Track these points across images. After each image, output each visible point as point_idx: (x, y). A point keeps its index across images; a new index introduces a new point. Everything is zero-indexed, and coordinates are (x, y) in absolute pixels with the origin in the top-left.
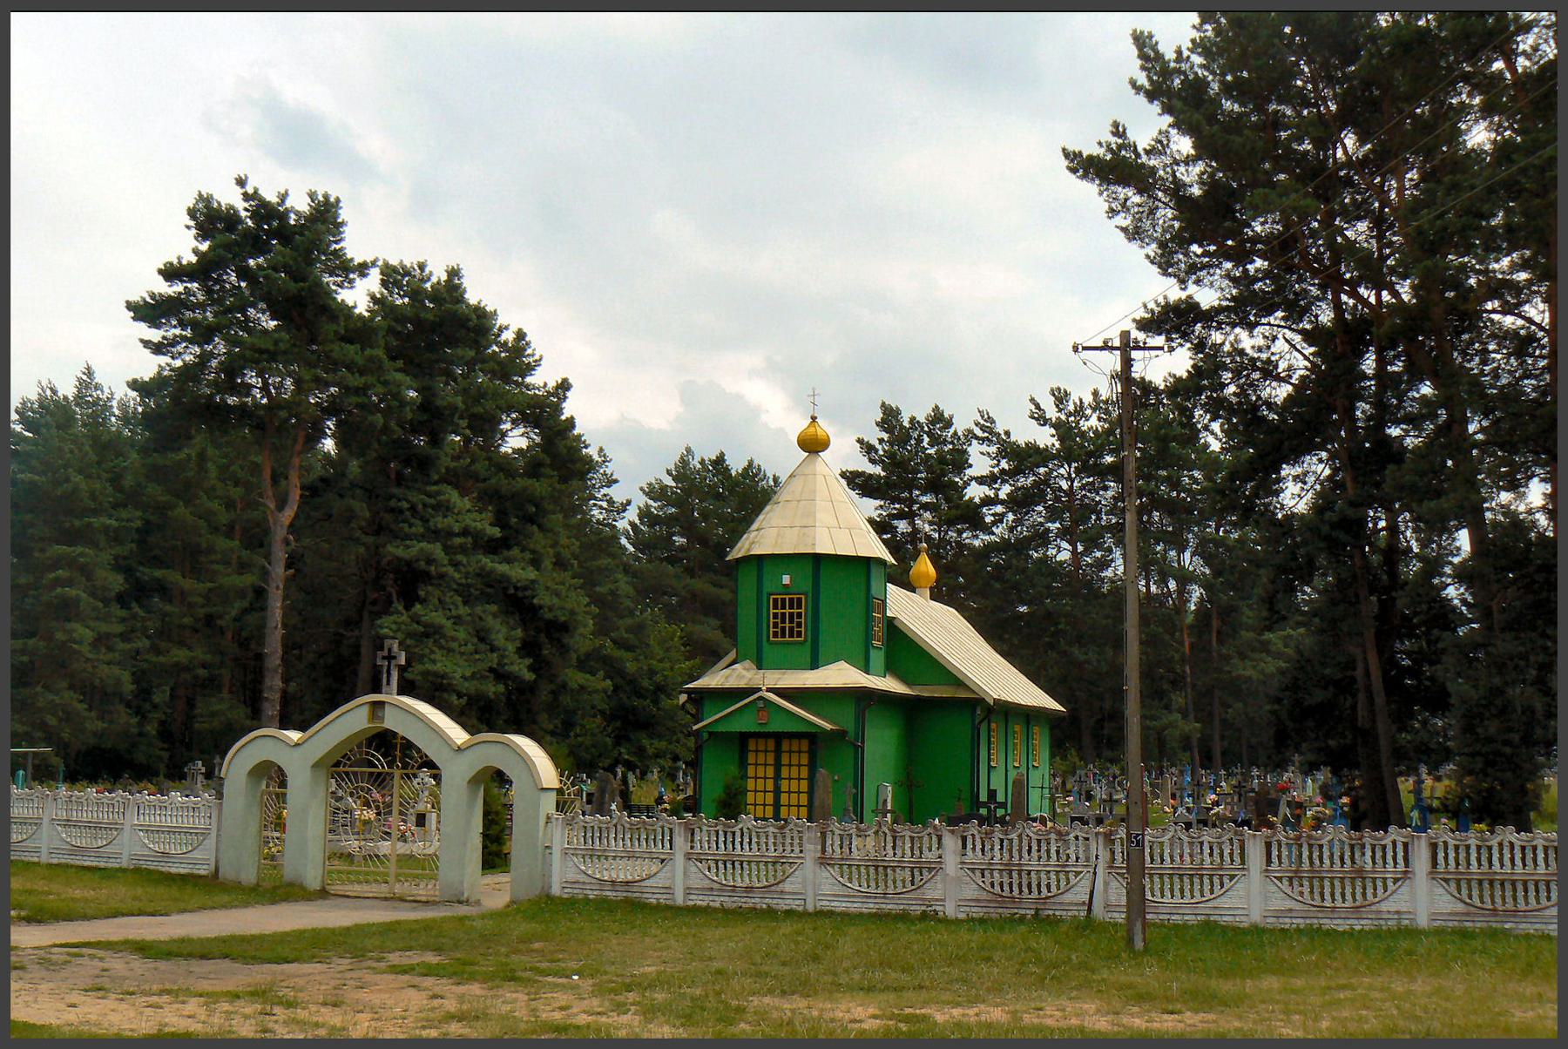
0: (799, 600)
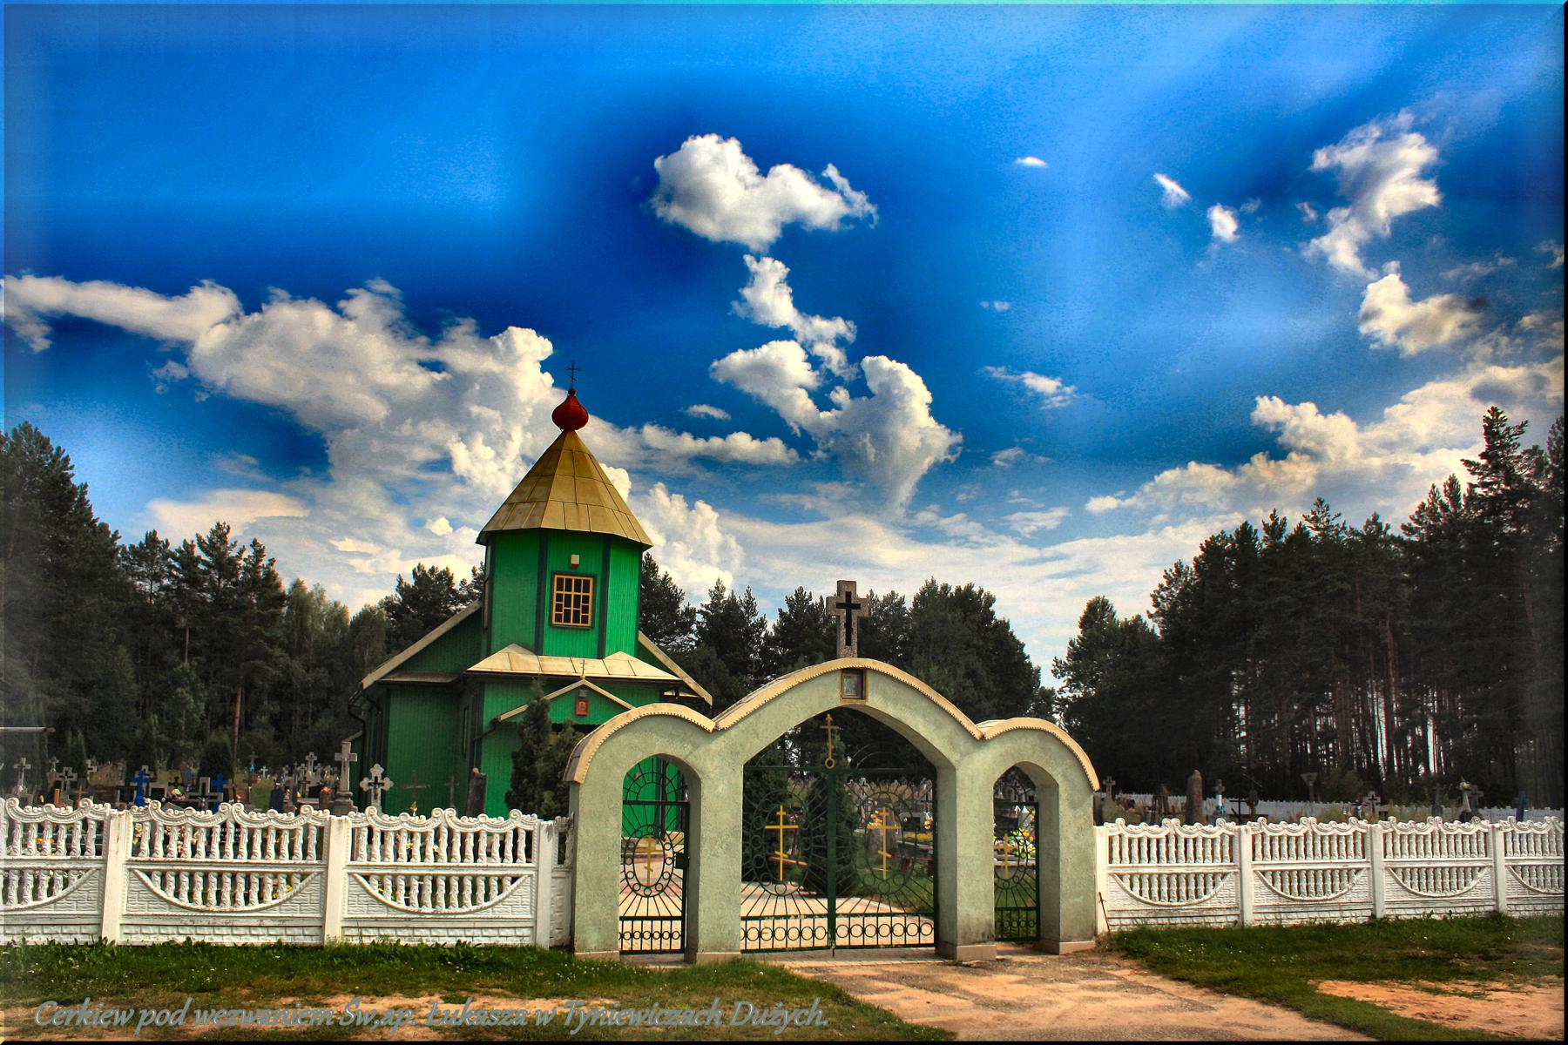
0: (587, 583)
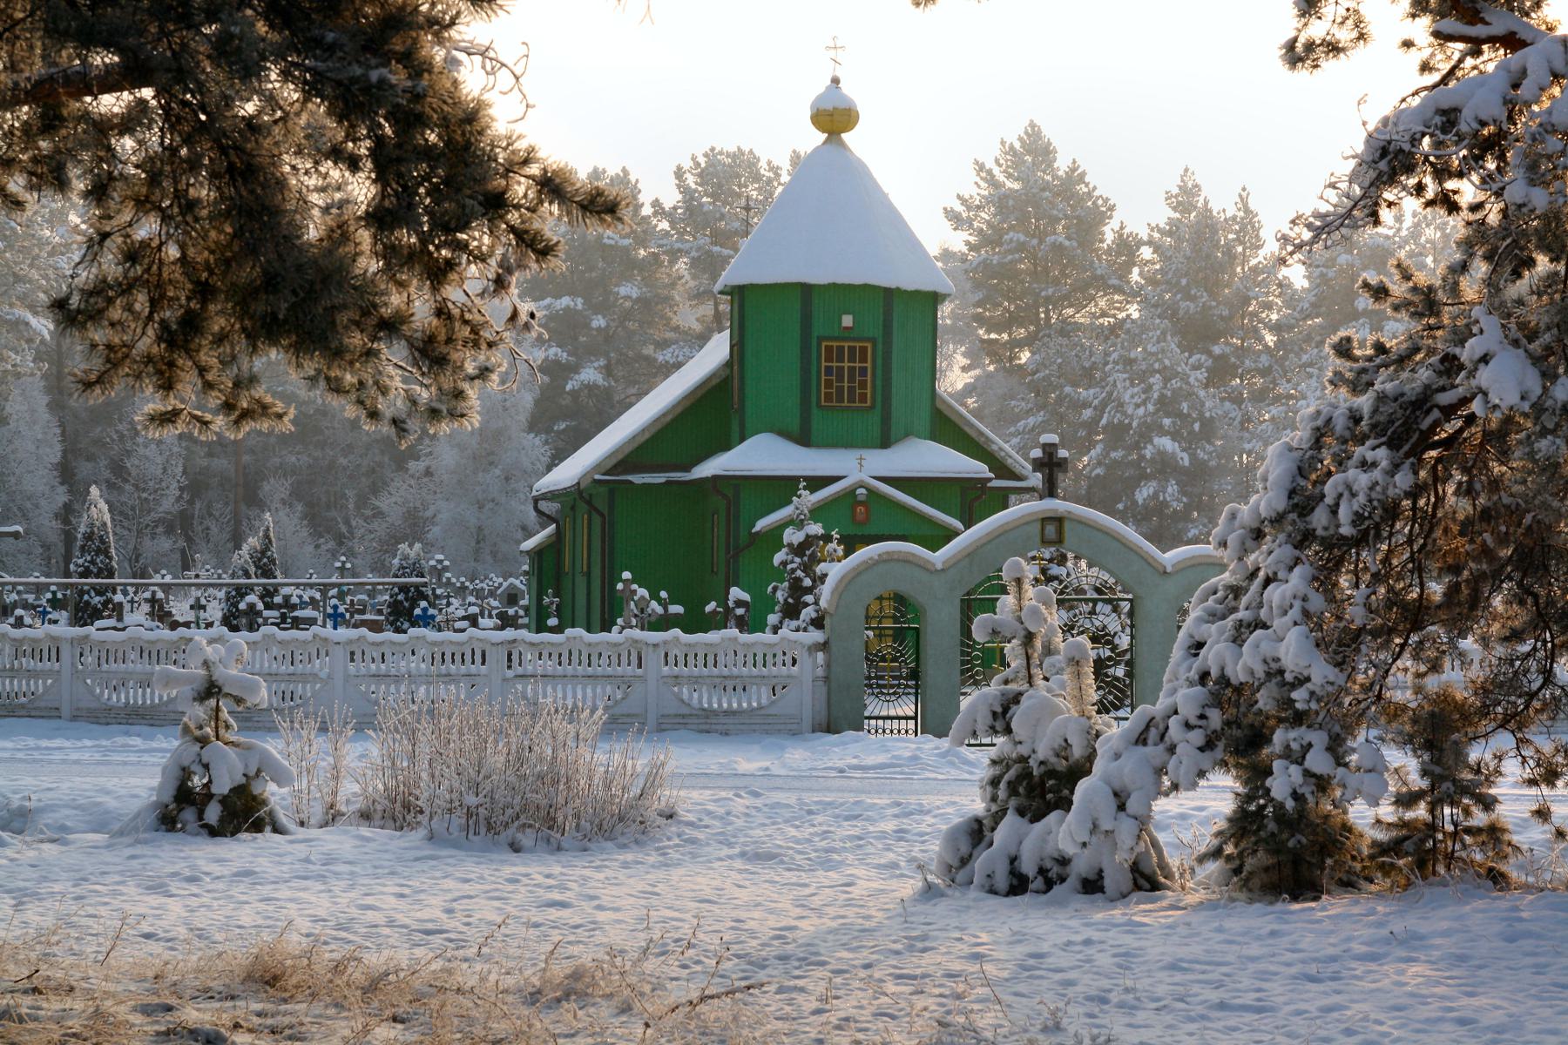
0: (864, 350)
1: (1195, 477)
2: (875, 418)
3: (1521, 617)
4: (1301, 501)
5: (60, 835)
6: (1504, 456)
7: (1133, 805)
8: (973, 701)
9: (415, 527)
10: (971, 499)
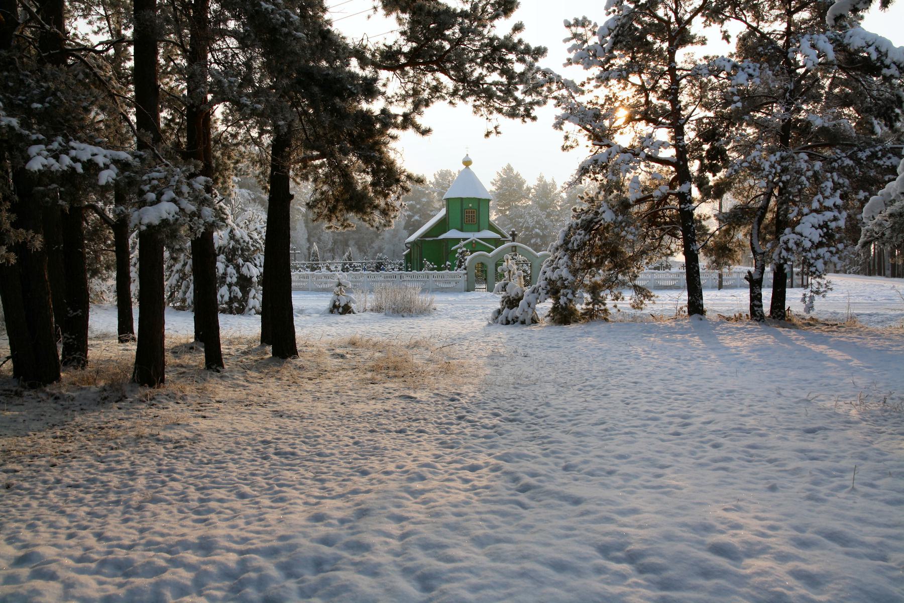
1: (544, 238)
2: (476, 226)
3: (611, 266)
4: (566, 242)
5: (309, 315)
6: (608, 233)
7: (532, 306)
8: (497, 285)
9: (380, 250)
10: (497, 243)
